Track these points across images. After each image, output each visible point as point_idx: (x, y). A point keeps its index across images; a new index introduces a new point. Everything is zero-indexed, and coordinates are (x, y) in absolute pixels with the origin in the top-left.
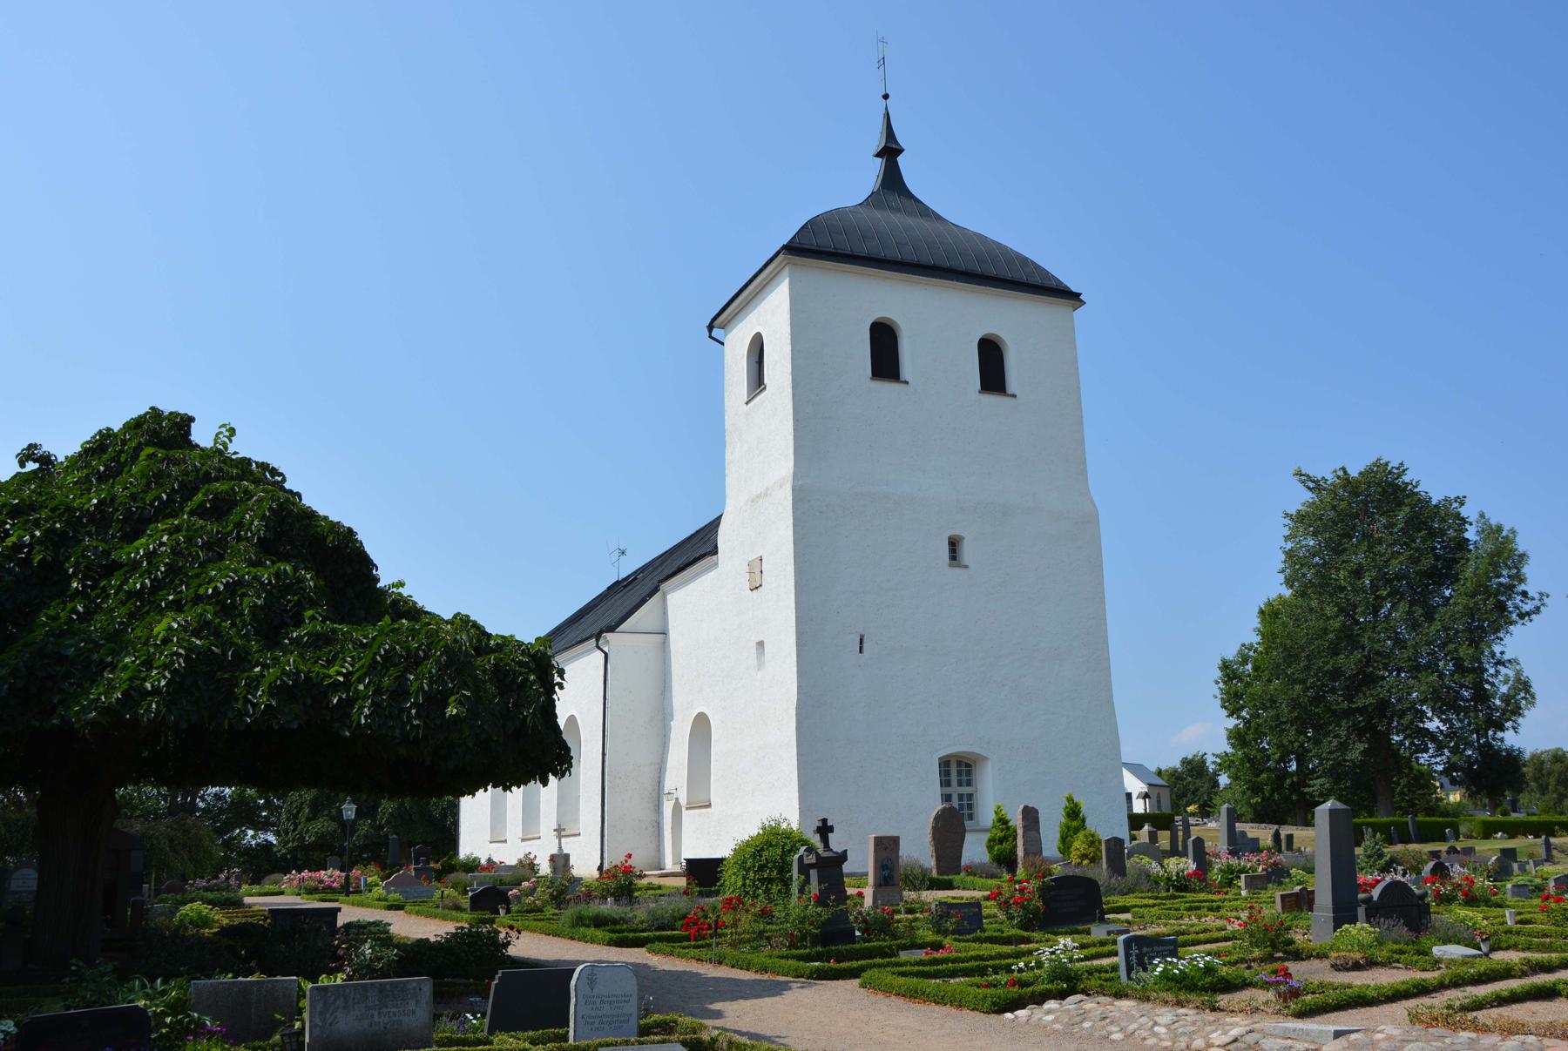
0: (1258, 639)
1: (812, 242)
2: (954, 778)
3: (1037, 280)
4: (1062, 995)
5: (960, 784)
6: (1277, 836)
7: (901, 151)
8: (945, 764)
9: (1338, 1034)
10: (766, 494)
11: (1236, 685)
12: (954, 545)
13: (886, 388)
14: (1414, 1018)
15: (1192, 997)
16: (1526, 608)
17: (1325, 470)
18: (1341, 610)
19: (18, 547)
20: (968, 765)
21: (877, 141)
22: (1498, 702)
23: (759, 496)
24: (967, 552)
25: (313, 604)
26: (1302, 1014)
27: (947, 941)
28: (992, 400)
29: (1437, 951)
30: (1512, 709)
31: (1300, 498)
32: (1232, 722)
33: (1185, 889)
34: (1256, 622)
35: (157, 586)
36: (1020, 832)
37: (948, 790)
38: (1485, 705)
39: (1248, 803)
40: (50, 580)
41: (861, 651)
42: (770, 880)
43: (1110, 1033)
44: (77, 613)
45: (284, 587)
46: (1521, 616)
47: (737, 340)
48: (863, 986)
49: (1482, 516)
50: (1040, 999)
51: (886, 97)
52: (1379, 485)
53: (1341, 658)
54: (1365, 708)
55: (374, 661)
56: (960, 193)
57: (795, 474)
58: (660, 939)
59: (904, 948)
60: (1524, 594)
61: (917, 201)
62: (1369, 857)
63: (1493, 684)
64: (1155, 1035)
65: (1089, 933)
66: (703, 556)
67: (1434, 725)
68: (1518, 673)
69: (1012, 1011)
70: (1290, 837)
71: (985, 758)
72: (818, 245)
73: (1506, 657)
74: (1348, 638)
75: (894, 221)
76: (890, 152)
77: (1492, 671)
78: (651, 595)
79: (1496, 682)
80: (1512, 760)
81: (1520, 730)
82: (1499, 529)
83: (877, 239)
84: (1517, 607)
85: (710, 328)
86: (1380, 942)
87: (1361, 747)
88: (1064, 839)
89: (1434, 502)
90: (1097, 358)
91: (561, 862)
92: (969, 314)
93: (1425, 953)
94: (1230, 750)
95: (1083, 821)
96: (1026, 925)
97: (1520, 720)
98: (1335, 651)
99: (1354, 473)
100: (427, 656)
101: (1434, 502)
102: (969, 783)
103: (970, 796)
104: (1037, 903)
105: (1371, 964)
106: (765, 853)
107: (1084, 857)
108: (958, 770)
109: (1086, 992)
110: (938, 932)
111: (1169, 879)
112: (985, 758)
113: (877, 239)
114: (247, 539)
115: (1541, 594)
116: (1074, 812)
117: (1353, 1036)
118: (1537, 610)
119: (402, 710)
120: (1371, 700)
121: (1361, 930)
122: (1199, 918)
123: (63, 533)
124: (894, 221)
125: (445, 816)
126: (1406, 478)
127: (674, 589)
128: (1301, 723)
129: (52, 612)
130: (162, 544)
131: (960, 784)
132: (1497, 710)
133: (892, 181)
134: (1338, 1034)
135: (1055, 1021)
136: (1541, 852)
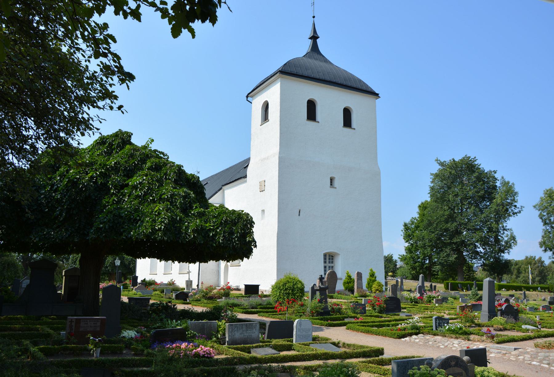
0: (418, 216)
1: (289, 70)
3: (364, 88)
4: (416, 334)
5: (329, 263)
6: (431, 285)
7: (318, 37)
8: (325, 255)
9: (515, 349)
10: (268, 158)
11: (409, 232)
12: (332, 180)
13: (311, 123)
14: (537, 346)
15: (461, 336)
16: (516, 211)
17: (447, 158)
18: (449, 208)
19: (92, 177)
20: (332, 256)
21: (310, 33)
22: (503, 243)
23: (265, 159)
24: (336, 183)
25: (195, 203)
26: (498, 343)
27: (358, 316)
28: (347, 130)
29: (524, 327)
30: (508, 246)
31: (436, 168)
32: (407, 245)
33: (416, 302)
34: (417, 210)
35: (146, 194)
36: (356, 280)
37: (326, 265)
38: (497, 244)
39: (411, 274)
40: (103, 189)
42: (289, 294)
43: (439, 346)
44: (115, 201)
45: (186, 196)
46: (514, 214)
47: (258, 102)
48: (348, 329)
49: (503, 178)
50: (411, 335)
51: (314, 17)
52: (466, 164)
53: (449, 225)
54: (457, 242)
55: (221, 222)
56: (338, 55)
57: (280, 152)
58: (264, 312)
59: (346, 318)
60: (515, 206)
61: (323, 56)
62: (473, 295)
63: (502, 237)
64: (455, 347)
65: (399, 315)
66: (241, 178)
67: (480, 249)
68: (512, 234)
69: (403, 338)
70: (435, 286)
71: (337, 254)
72: (289, 71)
73: (507, 228)
74: (451, 218)
75: (314, 63)
76: (314, 37)
77: (502, 232)
78: (219, 190)
79: (503, 236)
80: (508, 263)
81: (510, 253)
82: (508, 183)
83: (309, 70)
84: (512, 211)
85: (247, 97)
86: (506, 322)
87: (455, 256)
88: (369, 284)
89: (486, 172)
90: (382, 116)
91: (190, 283)
93: (520, 327)
94: (405, 254)
95: (376, 278)
96: (381, 312)
97: (511, 250)
98: (447, 222)
99: (457, 160)
100: (238, 222)
101: (486, 172)
102: (332, 263)
104: (383, 305)
105: (505, 329)
106: (287, 285)
107: (377, 290)
108: (329, 258)
109: (423, 333)
110: (355, 313)
111: (411, 299)
113: (309, 70)
114: (170, 179)
115: (522, 207)
116: (372, 275)
117: (520, 350)
118: (520, 212)
119: (233, 238)
120: (459, 240)
121: (499, 319)
122: (431, 312)
123: (105, 174)
124: (314, 63)
125: (130, 264)
126: (476, 163)
127: (228, 189)
128: (432, 247)
129: (107, 200)
130: (144, 180)
131: (329, 263)
132: (503, 246)
133: (315, 48)
134: (515, 349)
135: (420, 341)
136: (523, 296)
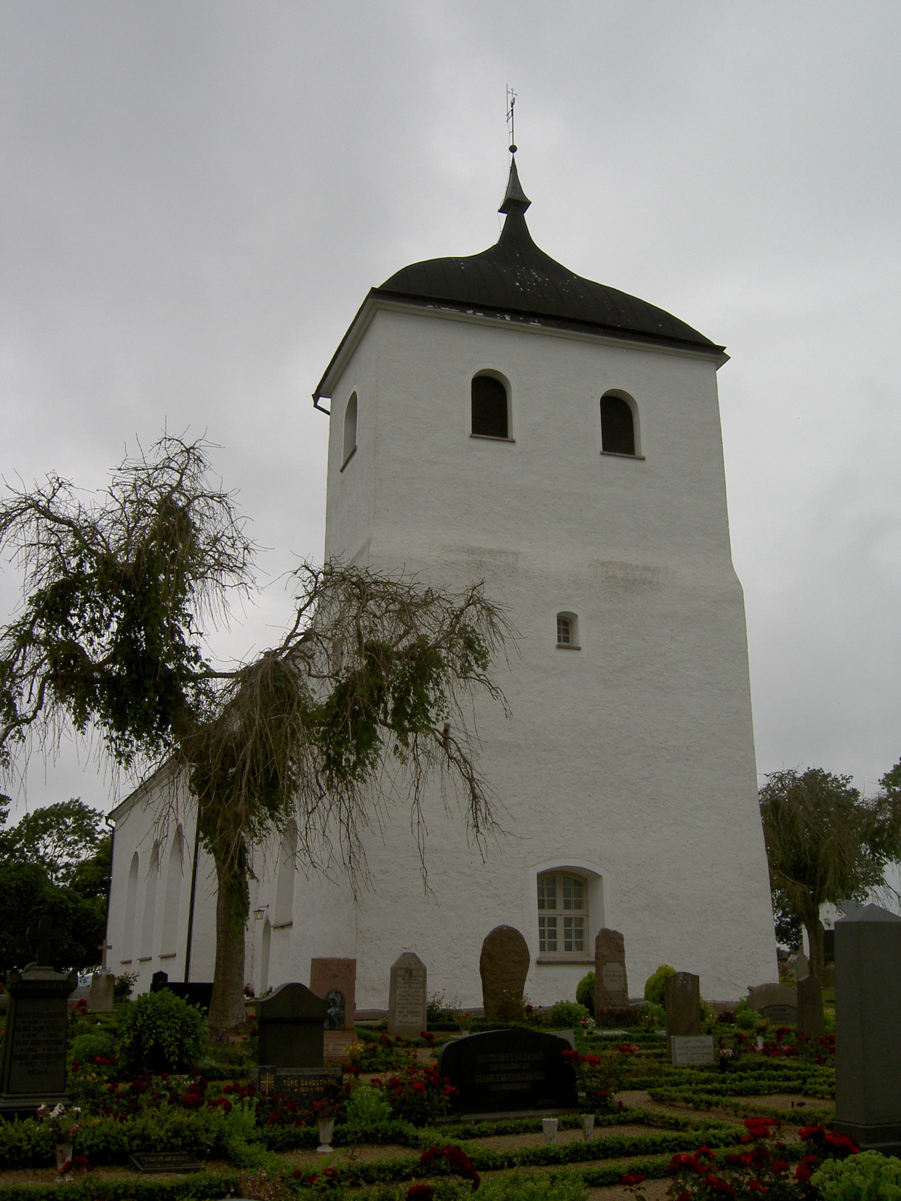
2: (561, 940)
5: (567, 906)
7: (527, 204)
21: (499, 197)
24: (582, 633)
41: (342, 471)
76: (515, 205)
85: (316, 397)
92: (587, 370)
102: (579, 906)
103: (580, 921)
112: (598, 877)
